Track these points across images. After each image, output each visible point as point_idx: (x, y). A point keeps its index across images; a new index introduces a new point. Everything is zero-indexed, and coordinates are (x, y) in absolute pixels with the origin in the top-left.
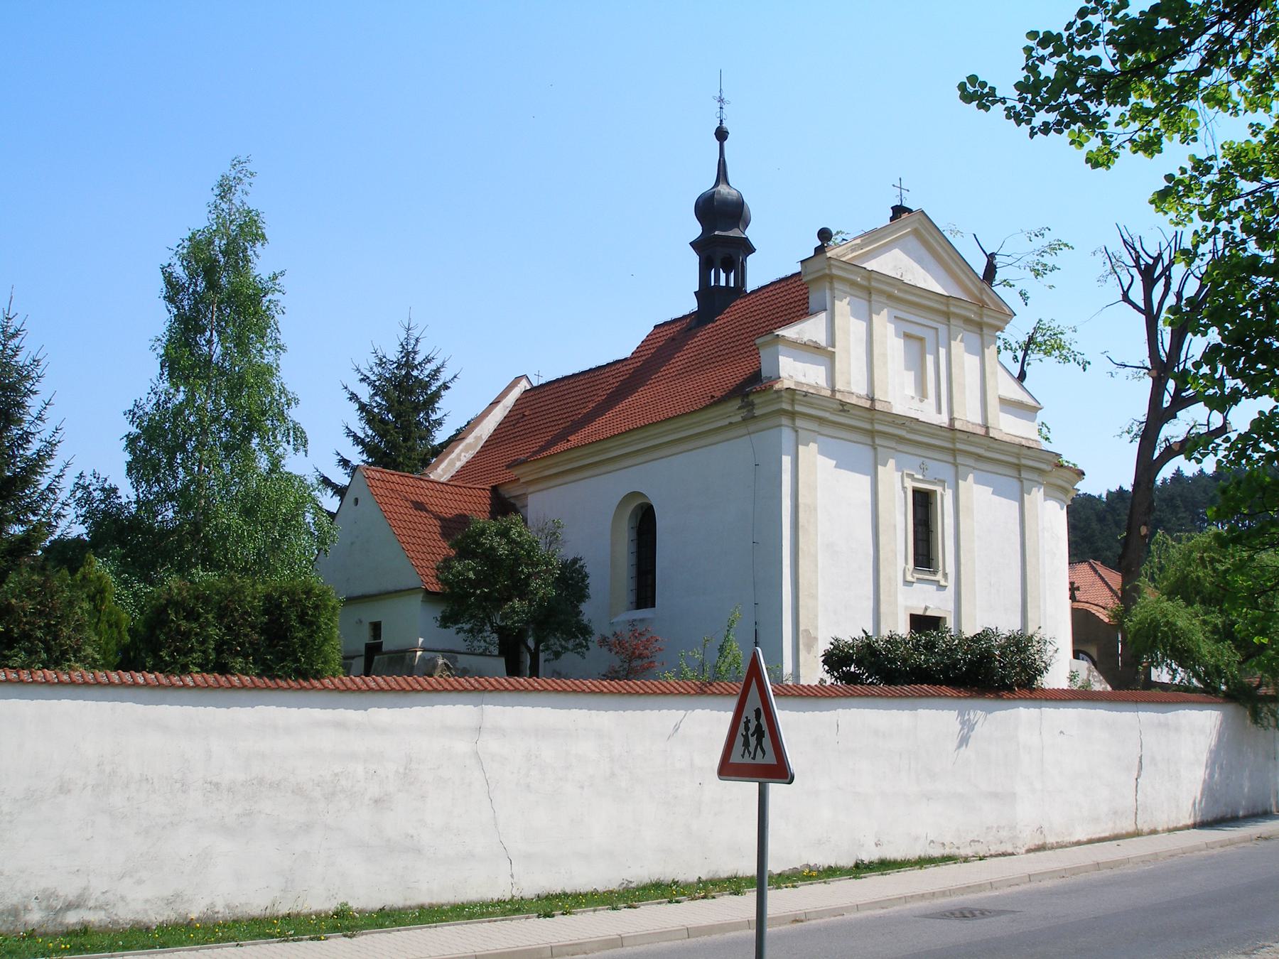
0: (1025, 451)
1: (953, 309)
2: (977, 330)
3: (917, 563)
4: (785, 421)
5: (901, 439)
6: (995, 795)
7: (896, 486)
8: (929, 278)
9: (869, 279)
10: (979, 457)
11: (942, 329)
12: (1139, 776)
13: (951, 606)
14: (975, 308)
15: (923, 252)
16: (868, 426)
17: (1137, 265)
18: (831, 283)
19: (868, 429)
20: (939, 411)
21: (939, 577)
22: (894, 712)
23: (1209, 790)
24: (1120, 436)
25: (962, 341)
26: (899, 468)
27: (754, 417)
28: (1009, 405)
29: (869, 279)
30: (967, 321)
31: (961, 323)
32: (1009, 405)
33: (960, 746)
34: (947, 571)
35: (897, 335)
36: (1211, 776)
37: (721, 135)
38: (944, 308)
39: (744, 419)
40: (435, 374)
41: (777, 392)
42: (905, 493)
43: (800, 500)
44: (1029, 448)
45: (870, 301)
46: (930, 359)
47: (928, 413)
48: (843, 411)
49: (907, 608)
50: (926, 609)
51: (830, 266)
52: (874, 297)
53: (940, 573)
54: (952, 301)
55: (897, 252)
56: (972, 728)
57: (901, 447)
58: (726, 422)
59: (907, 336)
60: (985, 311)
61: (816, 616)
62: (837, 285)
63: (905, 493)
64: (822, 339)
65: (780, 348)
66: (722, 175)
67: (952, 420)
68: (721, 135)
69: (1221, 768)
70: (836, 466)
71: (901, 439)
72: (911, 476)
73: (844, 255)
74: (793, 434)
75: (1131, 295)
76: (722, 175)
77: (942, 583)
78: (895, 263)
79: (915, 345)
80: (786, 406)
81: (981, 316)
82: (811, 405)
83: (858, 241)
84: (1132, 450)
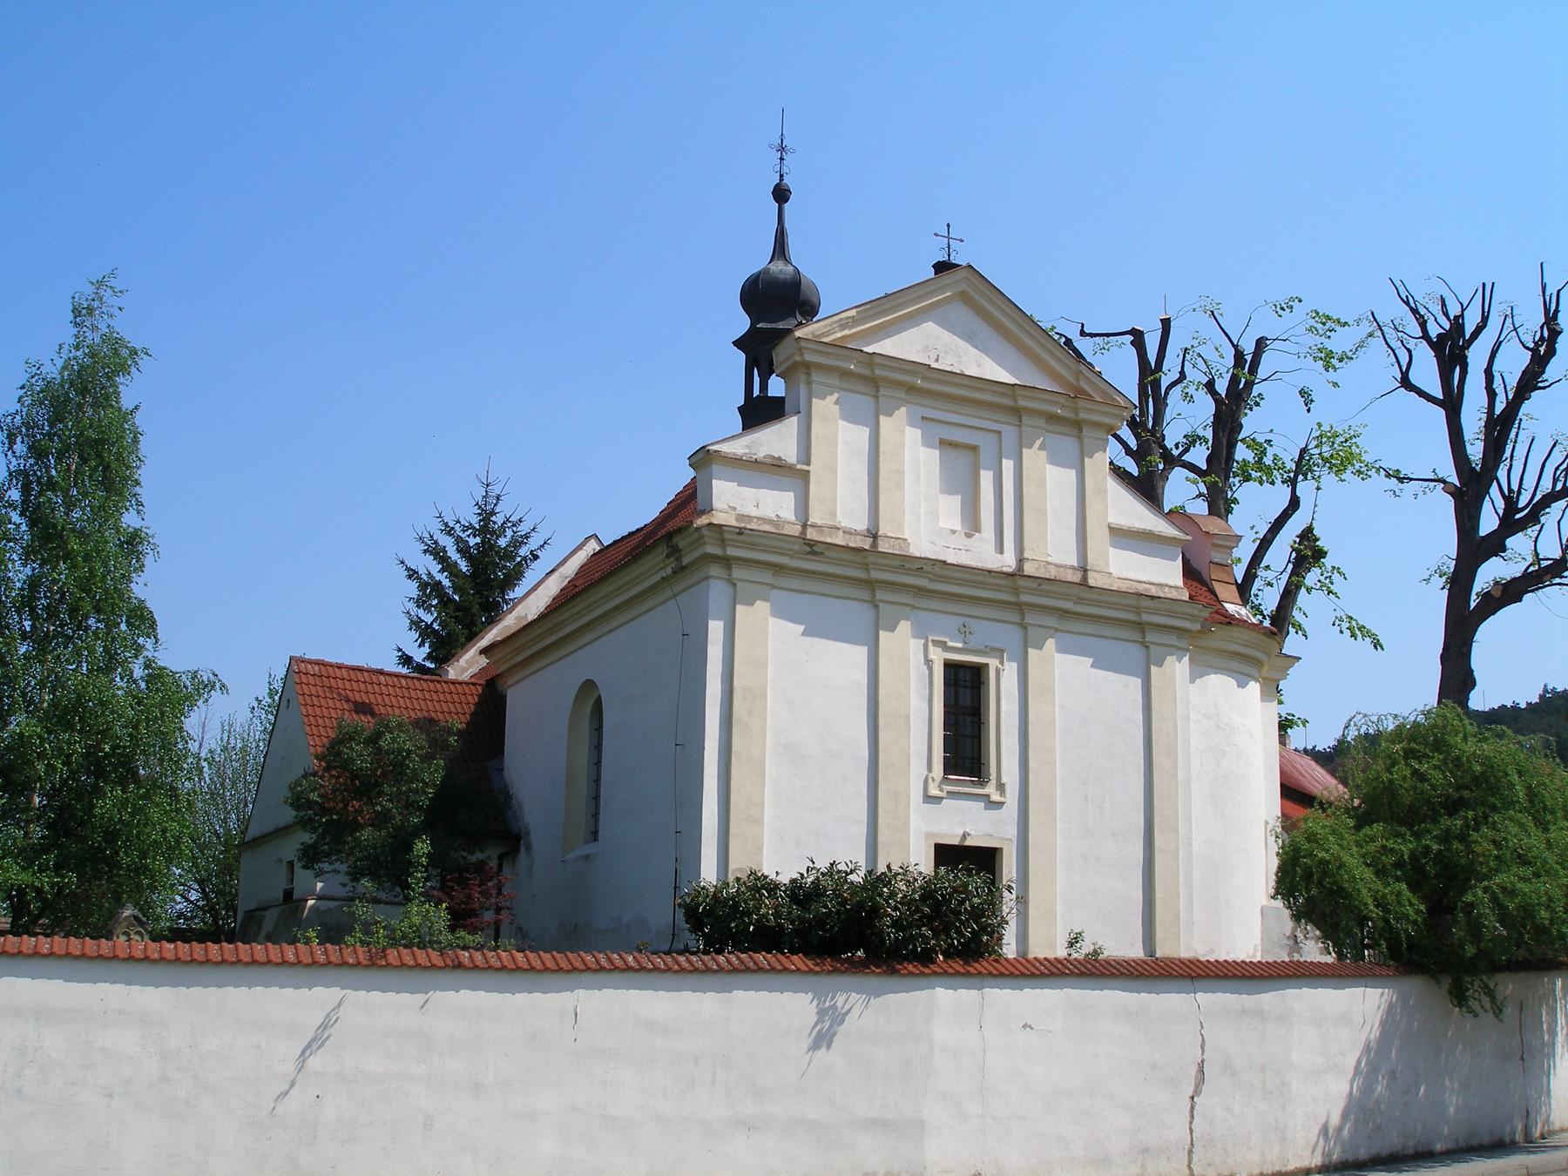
0: (1148, 603)
1: (1022, 403)
2: (1074, 432)
3: (951, 766)
4: (715, 570)
5: (920, 591)
6: (882, 1125)
7: (913, 663)
8: (986, 361)
9: (871, 366)
10: (1065, 614)
11: (1009, 432)
12: (1197, 1091)
13: (1012, 831)
14: (1062, 400)
15: (978, 325)
16: (861, 574)
17: (1425, 336)
18: (809, 374)
19: (863, 580)
20: (1000, 548)
21: (990, 789)
22: (687, 994)
23: (1359, 1109)
24: (1427, 580)
25: (1042, 447)
26: (917, 634)
27: (683, 568)
28: (1123, 536)
29: (871, 366)
30: (1052, 418)
31: (1041, 422)
32: (1123, 536)
33: (815, 1046)
34: (1004, 780)
35: (927, 442)
36: (1367, 1089)
37: (781, 194)
38: (1010, 403)
39: (675, 572)
40: (518, 542)
41: (698, 529)
42: (930, 669)
43: (736, 683)
44: (1152, 597)
45: (877, 397)
46: (986, 478)
47: (982, 553)
48: (813, 553)
49: (928, 835)
50: (964, 836)
51: (800, 349)
52: (882, 391)
53: (993, 782)
54: (1019, 391)
55: (930, 328)
56: (839, 1019)
57: (923, 603)
58: (657, 578)
59: (945, 444)
60: (1081, 404)
61: (760, 849)
62: (815, 377)
63: (930, 669)
64: (790, 454)
65: (715, 468)
66: (780, 249)
67: (1021, 561)
68: (781, 194)
69: (1392, 1075)
70: (804, 634)
71: (920, 591)
72: (943, 645)
73: (827, 334)
74: (729, 589)
75: (1414, 378)
76: (780, 249)
77: (996, 797)
78: (928, 343)
79: (963, 458)
80: (712, 549)
81: (1076, 410)
82: (752, 546)
83: (853, 313)
84: (1439, 599)
